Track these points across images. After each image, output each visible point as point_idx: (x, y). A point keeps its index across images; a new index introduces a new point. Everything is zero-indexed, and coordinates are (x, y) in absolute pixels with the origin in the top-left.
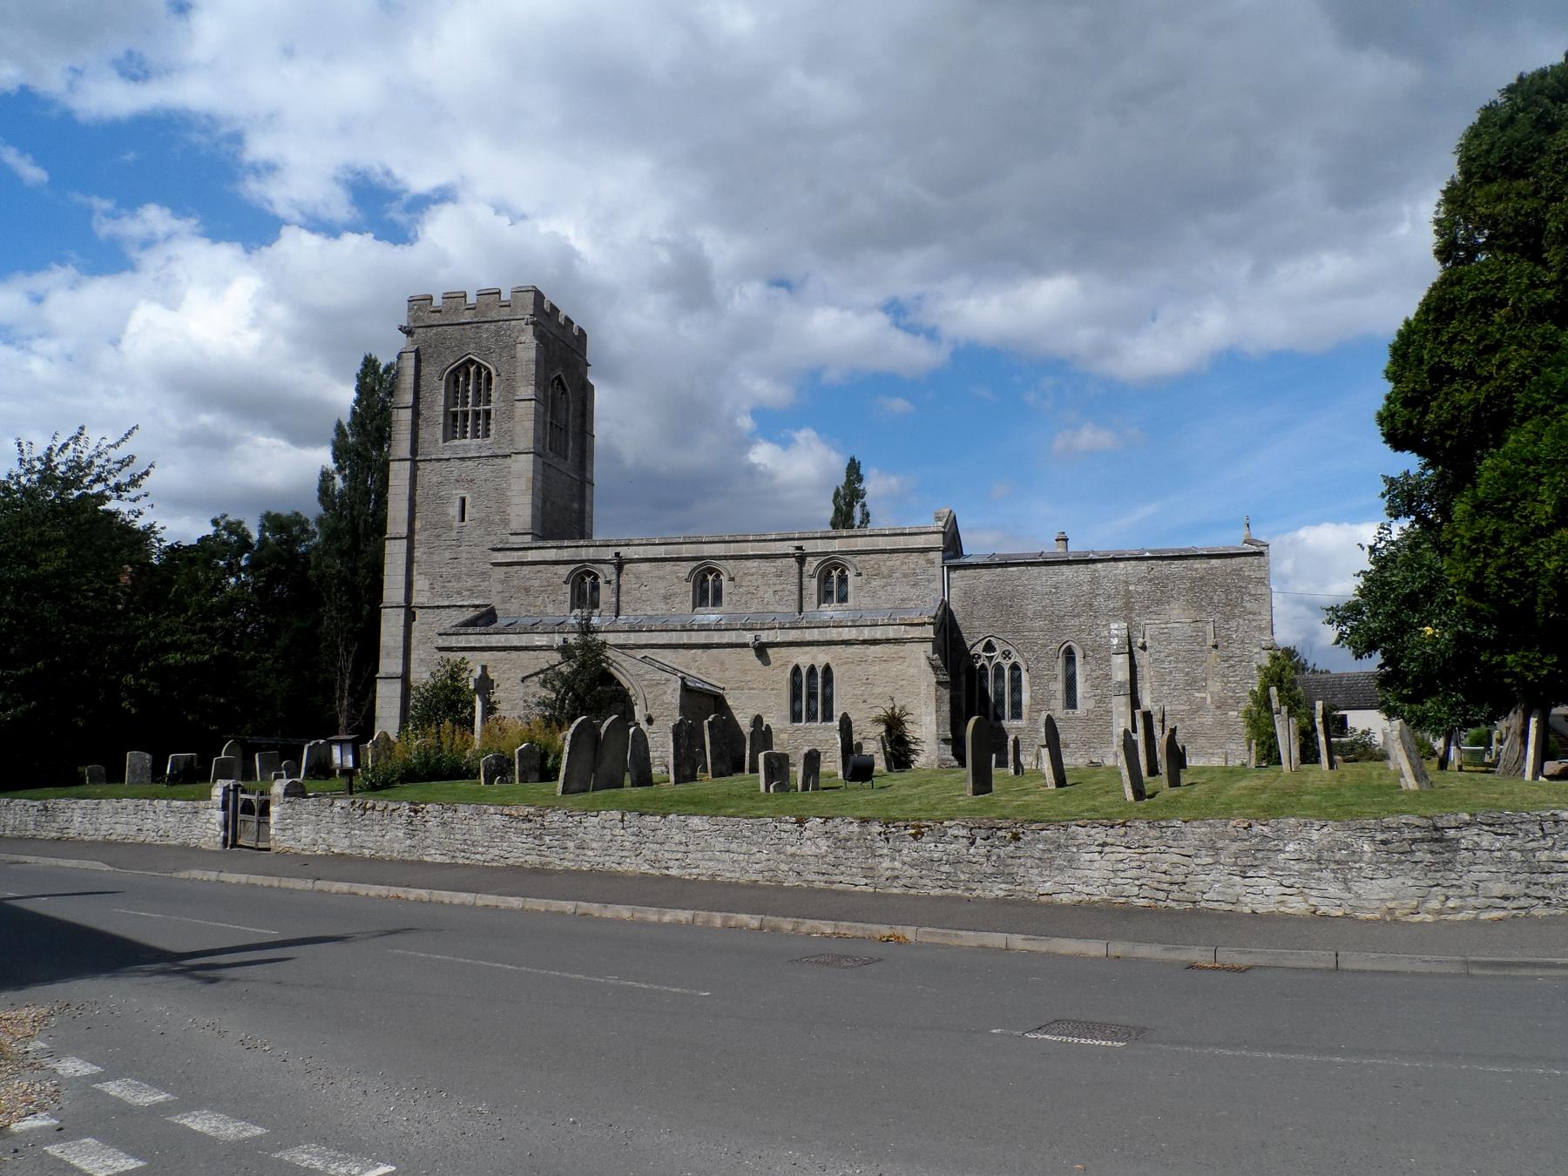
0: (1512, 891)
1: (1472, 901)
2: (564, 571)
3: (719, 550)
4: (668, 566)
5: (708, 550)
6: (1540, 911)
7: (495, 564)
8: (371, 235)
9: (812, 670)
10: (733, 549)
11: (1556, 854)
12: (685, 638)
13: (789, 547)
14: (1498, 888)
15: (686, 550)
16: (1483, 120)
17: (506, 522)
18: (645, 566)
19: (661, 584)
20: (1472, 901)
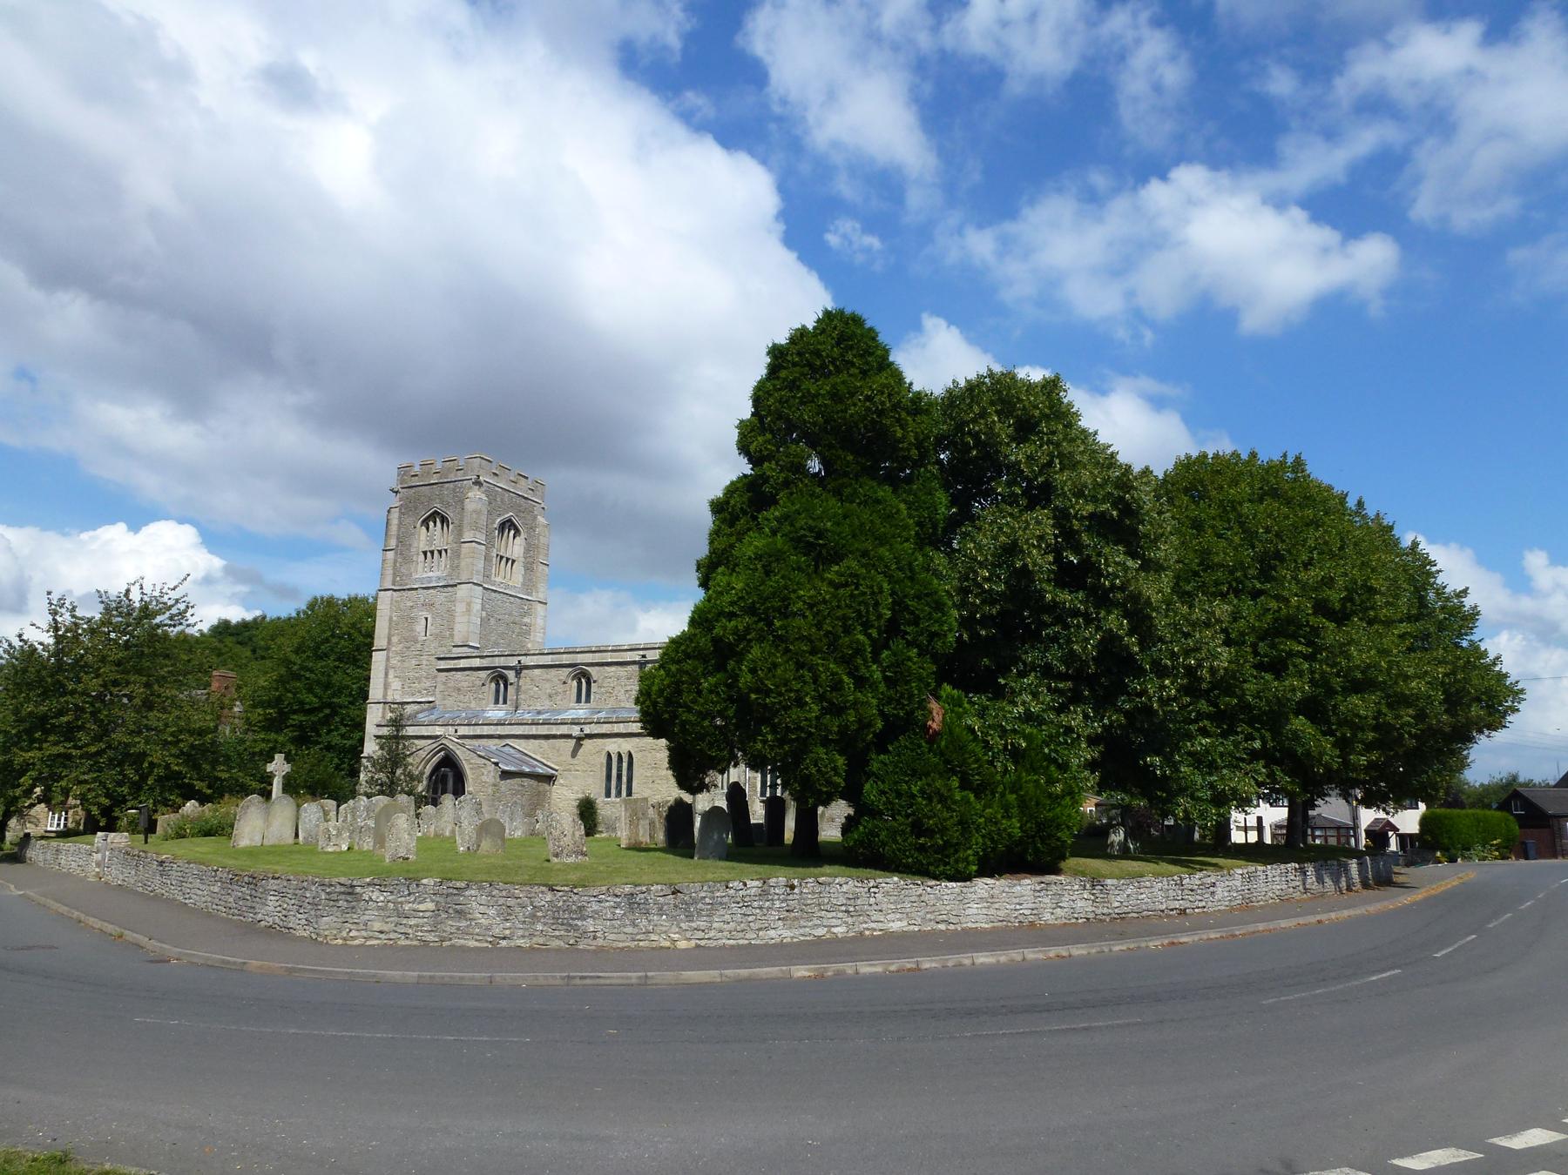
0: (385, 928)
1: (364, 933)
2: (483, 674)
3: (588, 658)
4: (553, 672)
5: (580, 658)
6: (403, 942)
7: (440, 670)
8: (810, 325)
9: (620, 755)
10: (597, 658)
11: (415, 906)
12: (534, 730)
13: (636, 656)
14: (377, 926)
15: (566, 659)
16: (773, 370)
17: (452, 636)
18: (537, 671)
19: (548, 685)
20: (364, 933)
